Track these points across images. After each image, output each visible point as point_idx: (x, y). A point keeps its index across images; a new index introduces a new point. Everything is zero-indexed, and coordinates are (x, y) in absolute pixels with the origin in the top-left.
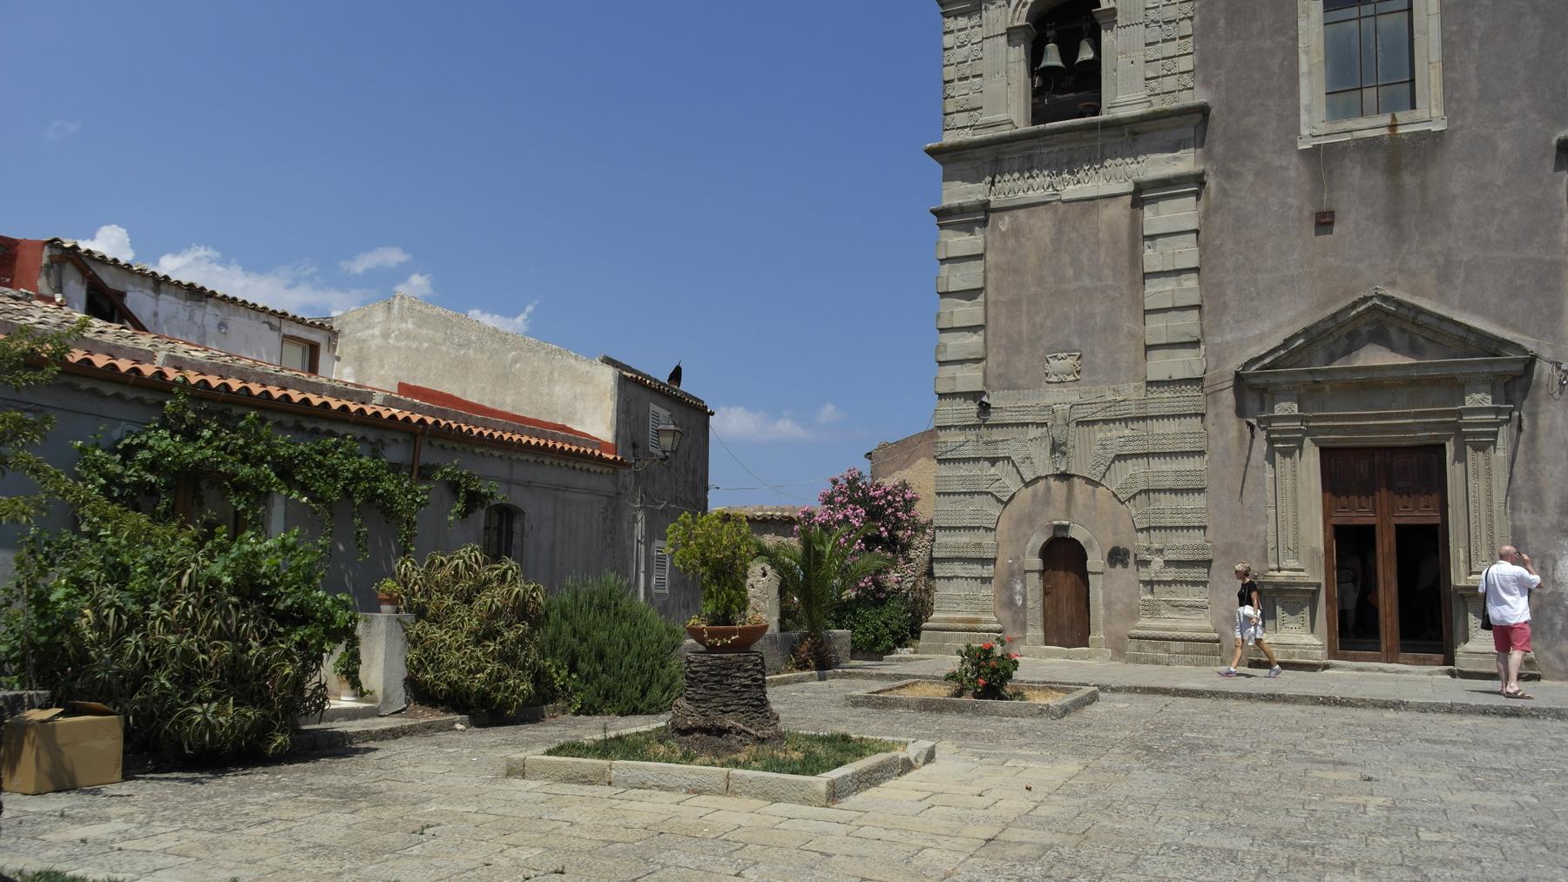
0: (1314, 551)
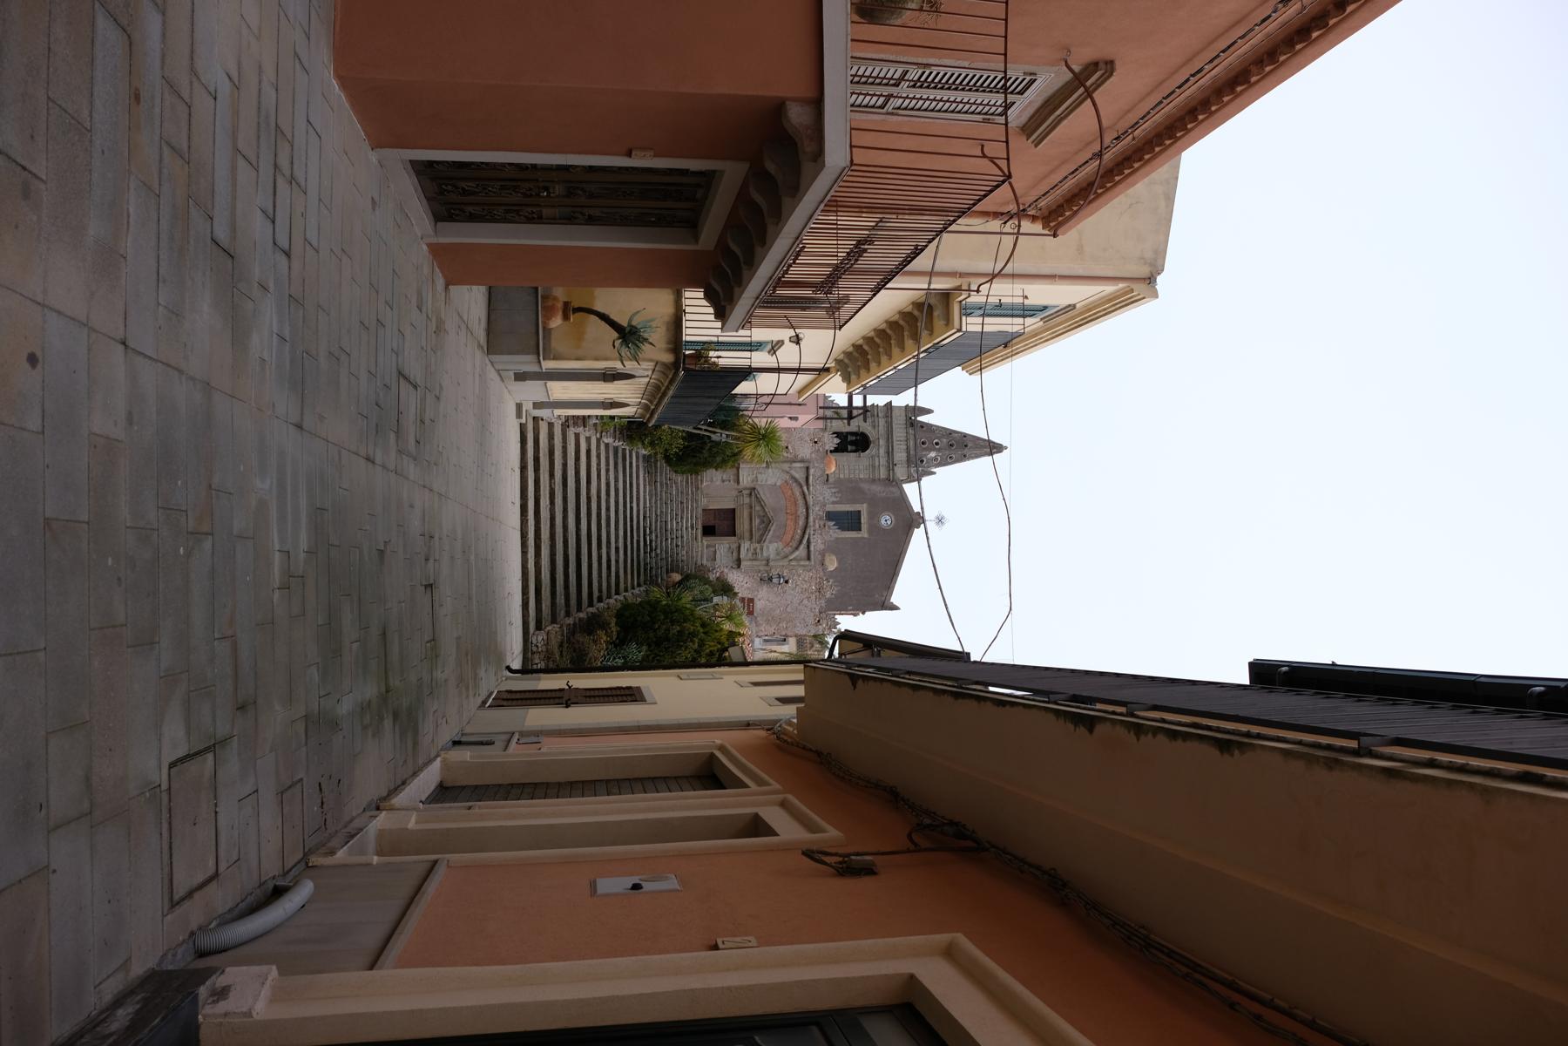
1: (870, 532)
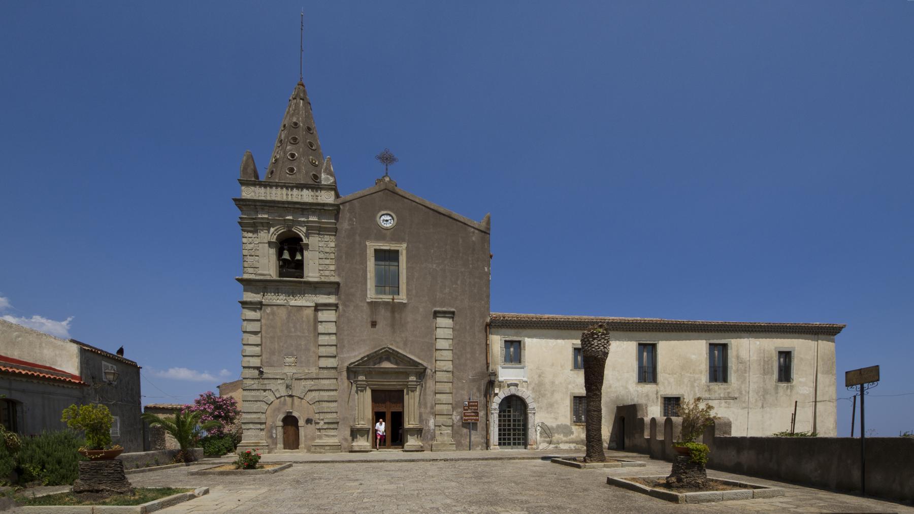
1: (399, 240)
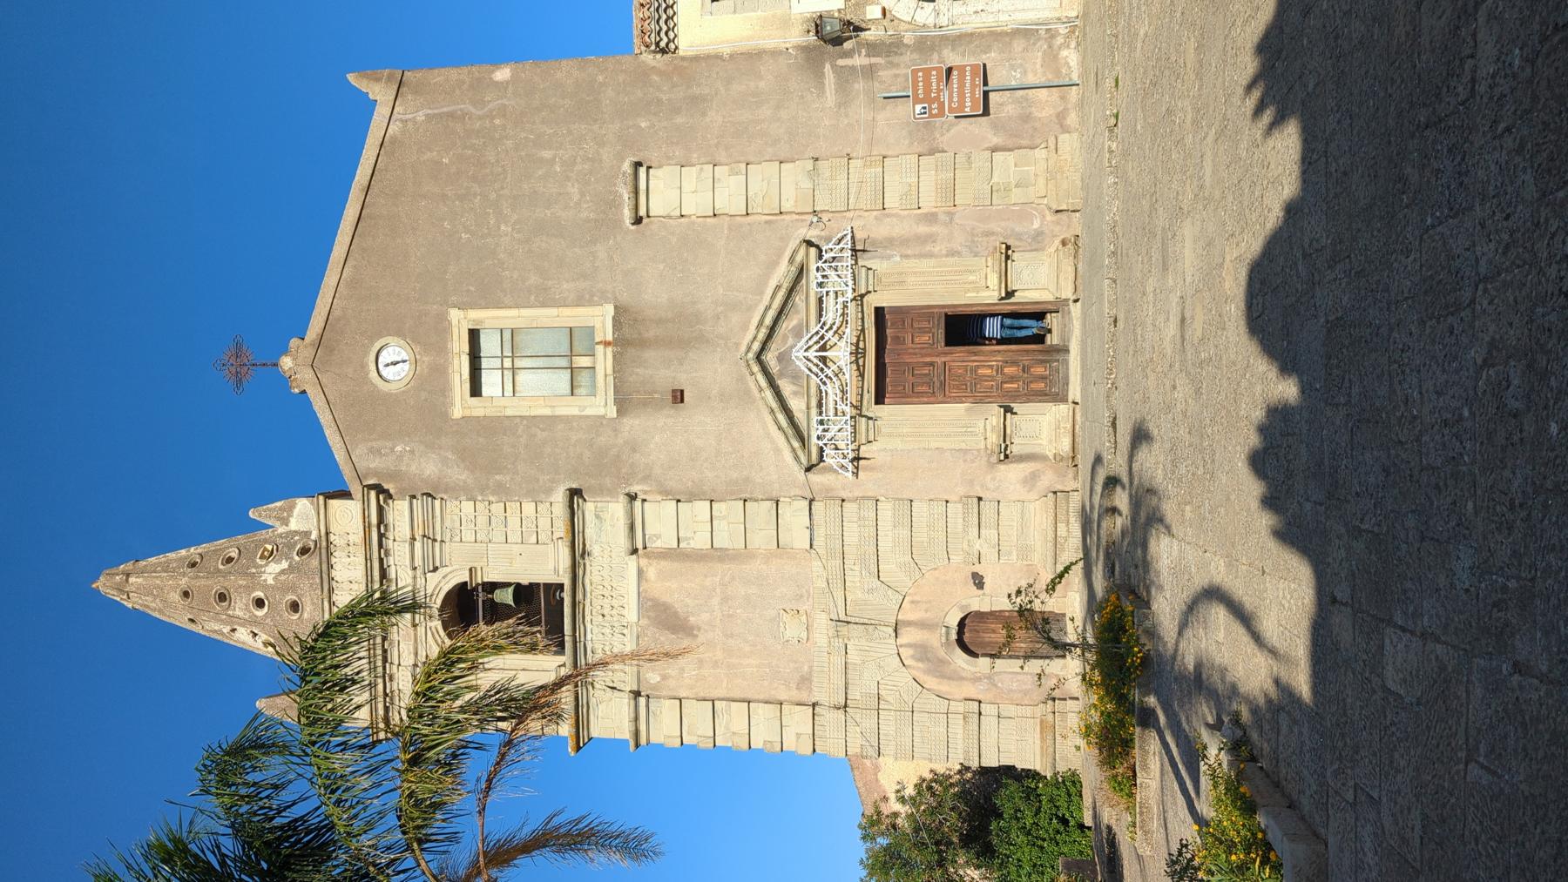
0: (968, 410)
1: (442, 328)
